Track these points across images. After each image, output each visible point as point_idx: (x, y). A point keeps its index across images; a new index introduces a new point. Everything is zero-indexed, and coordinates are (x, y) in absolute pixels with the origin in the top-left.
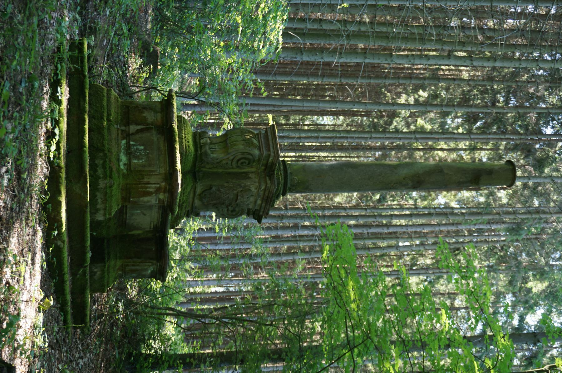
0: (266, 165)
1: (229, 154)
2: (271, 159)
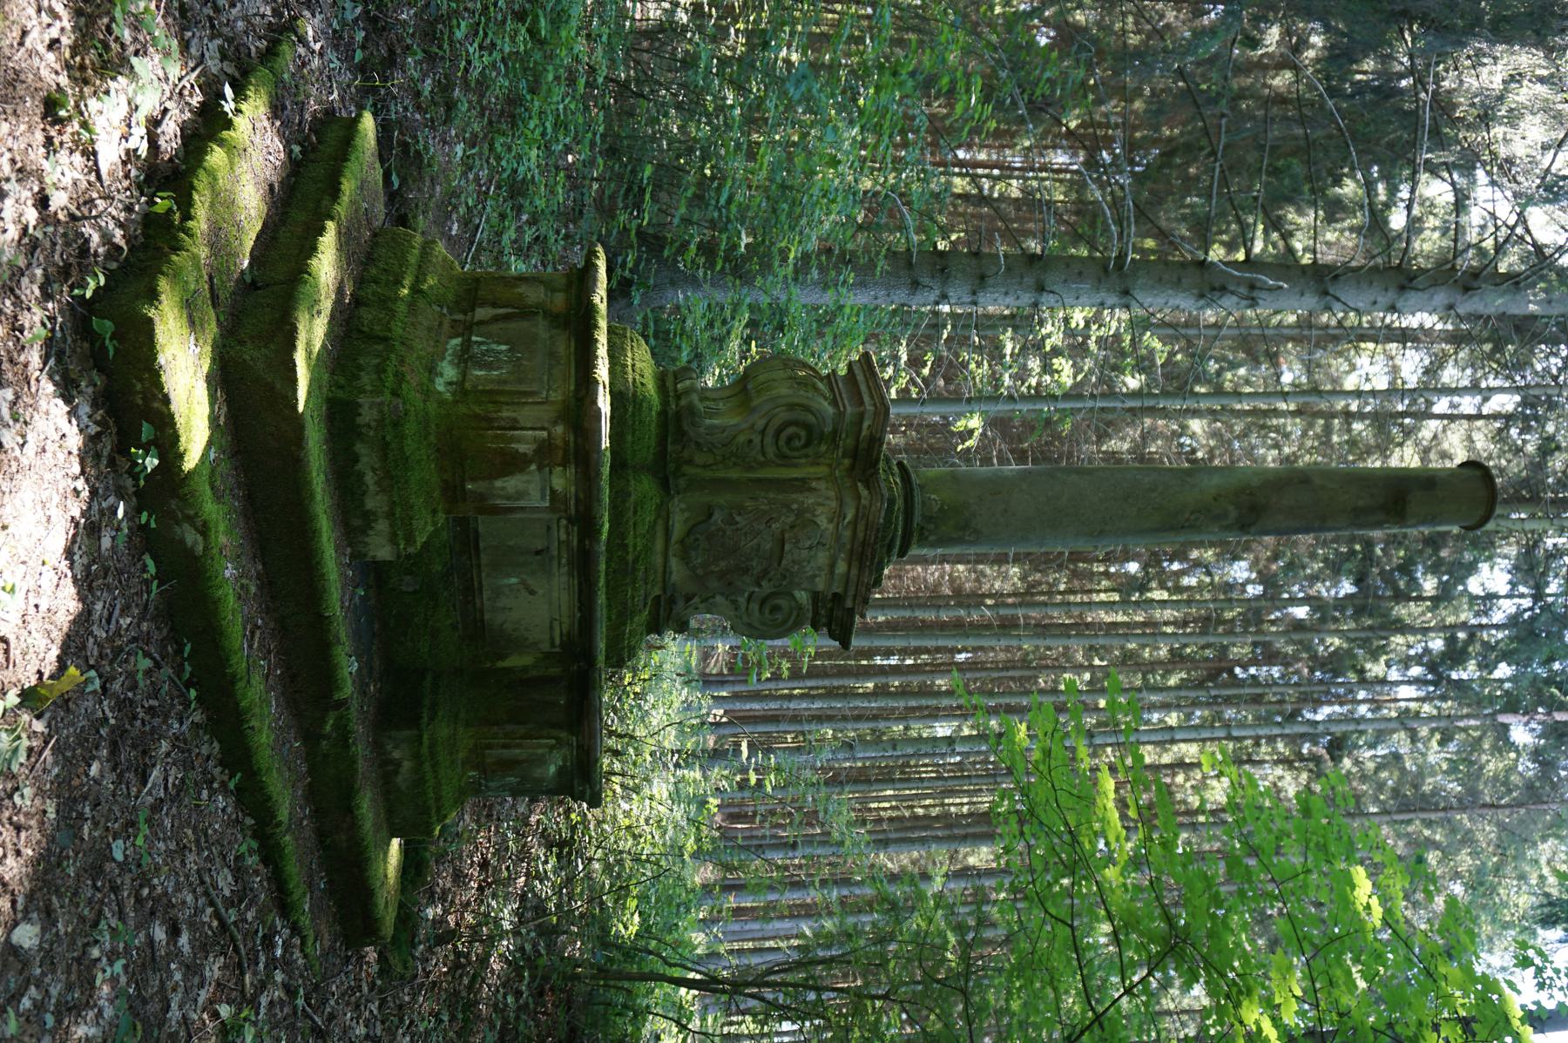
0: (854, 454)
1: (753, 410)
2: (866, 424)
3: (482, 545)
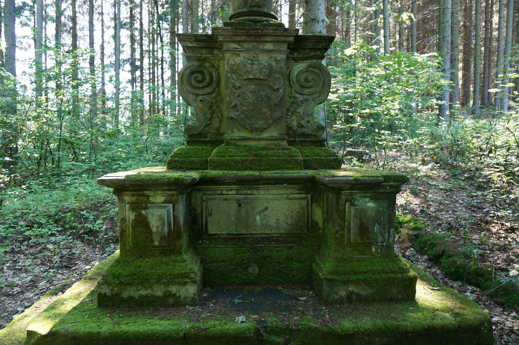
3: (234, 233)
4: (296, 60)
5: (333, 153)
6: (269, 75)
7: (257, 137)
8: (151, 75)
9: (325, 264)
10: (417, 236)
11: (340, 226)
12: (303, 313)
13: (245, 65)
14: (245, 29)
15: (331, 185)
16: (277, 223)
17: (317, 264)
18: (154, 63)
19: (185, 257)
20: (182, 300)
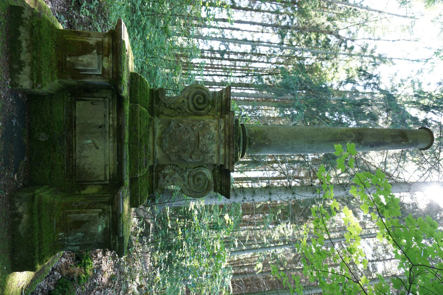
3: (77, 122)
4: (213, 172)
5: (143, 201)
6: (201, 151)
7: (156, 142)
8: (217, 66)
9: (48, 194)
10: (72, 280)
11: (82, 205)
12: (3, 176)
13: (209, 134)
14: (233, 134)
15: (116, 197)
16: (85, 157)
17: (47, 189)
18: (226, 69)
19: (56, 81)
20: (16, 76)
